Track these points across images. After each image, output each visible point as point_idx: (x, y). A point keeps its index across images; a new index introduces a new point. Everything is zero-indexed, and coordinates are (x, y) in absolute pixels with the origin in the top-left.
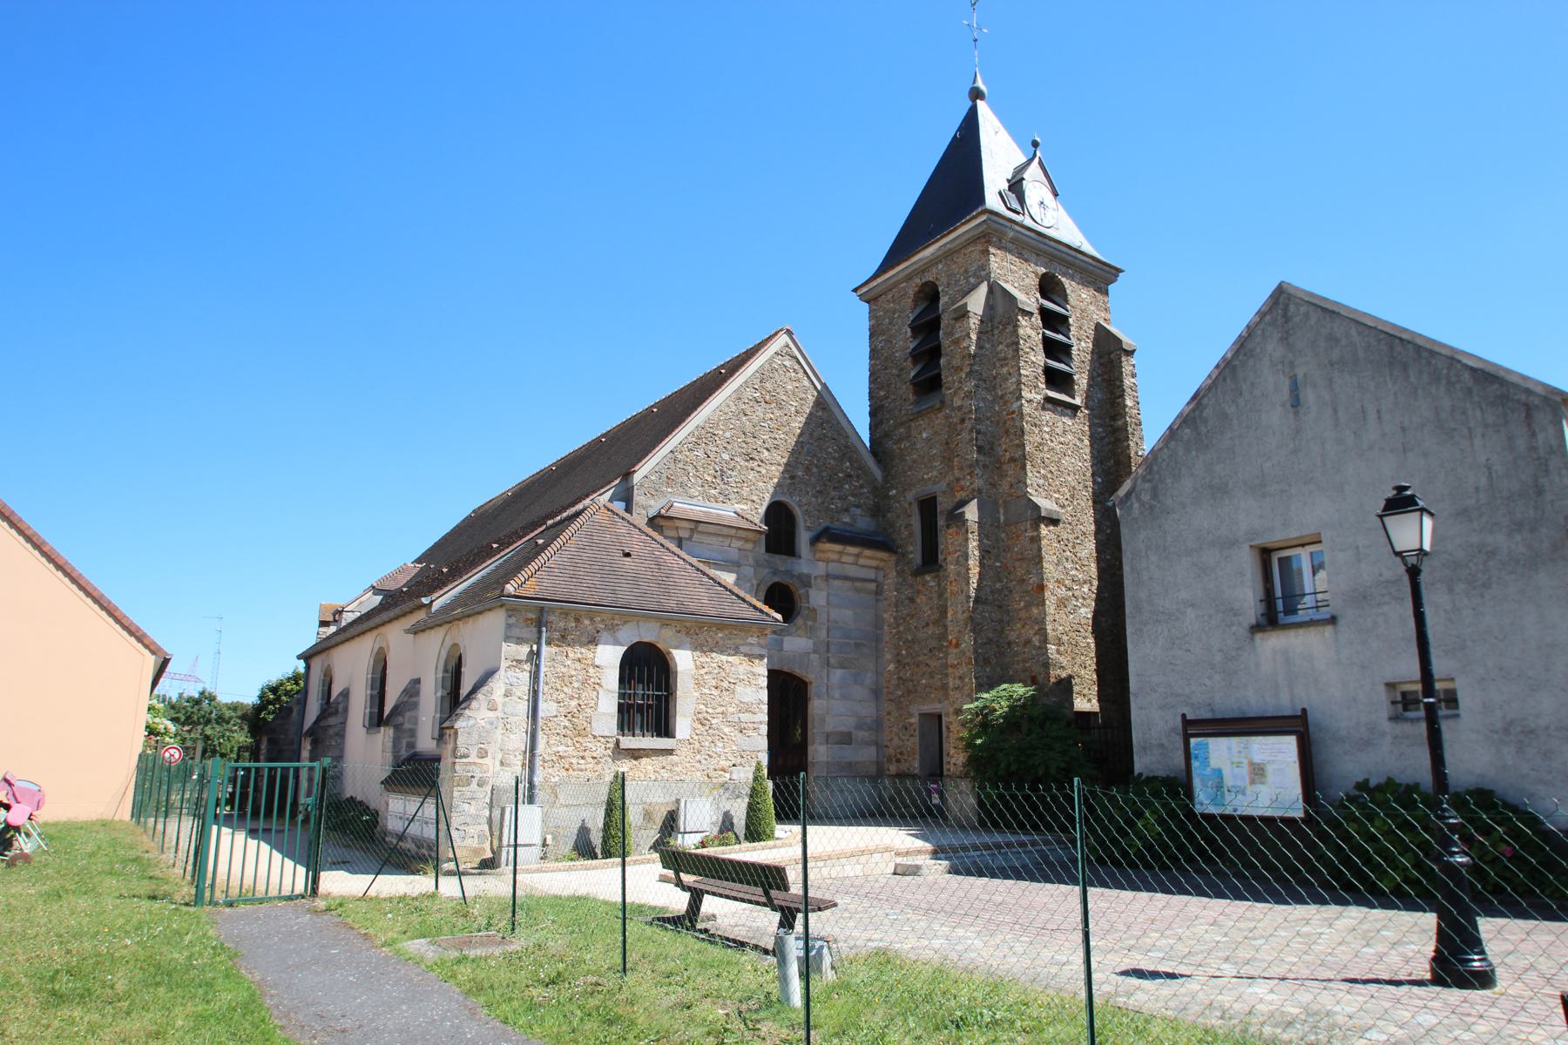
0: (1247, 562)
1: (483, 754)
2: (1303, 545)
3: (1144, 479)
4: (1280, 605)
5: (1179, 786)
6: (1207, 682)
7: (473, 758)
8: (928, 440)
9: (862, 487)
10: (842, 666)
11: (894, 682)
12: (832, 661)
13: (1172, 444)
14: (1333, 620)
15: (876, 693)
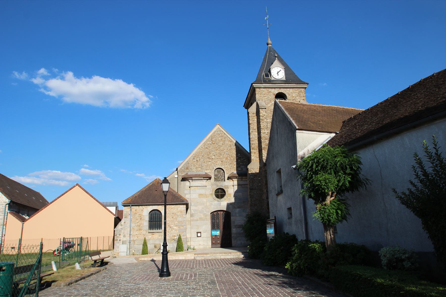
1: (120, 235)
10: (239, 208)
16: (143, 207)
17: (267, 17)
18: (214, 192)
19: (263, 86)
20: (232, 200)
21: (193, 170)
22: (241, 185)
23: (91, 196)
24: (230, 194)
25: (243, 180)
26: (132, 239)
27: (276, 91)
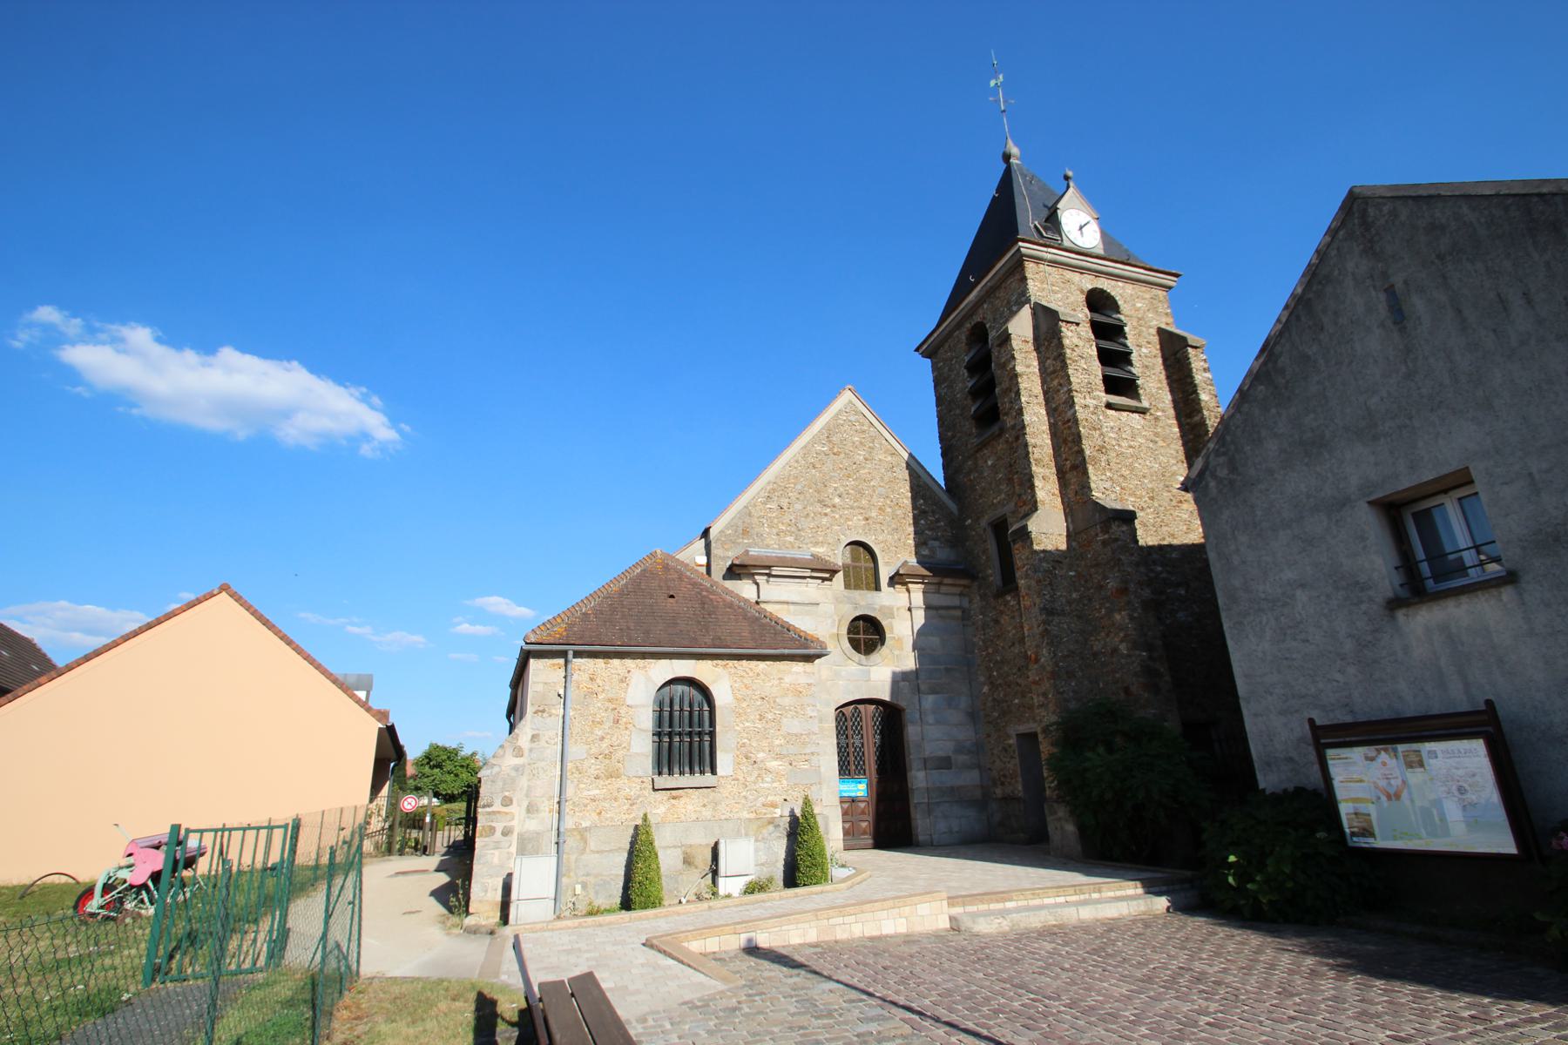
0: (1372, 526)
1: (507, 802)
2: (1445, 491)
3: (1217, 453)
4: (1425, 568)
5: (1323, 801)
6: (1338, 676)
7: (497, 807)
8: (993, 466)
9: (938, 521)
10: (933, 691)
11: (989, 704)
12: (923, 687)
13: (1245, 408)
14: (1511, 578)
15: (972, 716)
16: (629, 662)
17: (997, 78)
18: (844, 631)
19: (1049, 256)
20: (909, 663)
21: (768, 541)
22: (936, 608)
23: (284, 638)
24: (899, 640)
25: (944, 589)
26: (569, 823)
27: (1089, 283)
